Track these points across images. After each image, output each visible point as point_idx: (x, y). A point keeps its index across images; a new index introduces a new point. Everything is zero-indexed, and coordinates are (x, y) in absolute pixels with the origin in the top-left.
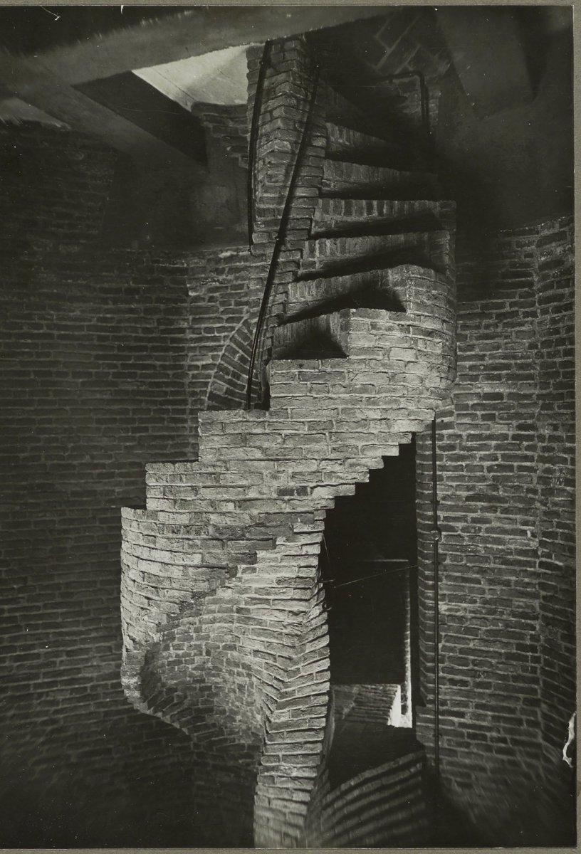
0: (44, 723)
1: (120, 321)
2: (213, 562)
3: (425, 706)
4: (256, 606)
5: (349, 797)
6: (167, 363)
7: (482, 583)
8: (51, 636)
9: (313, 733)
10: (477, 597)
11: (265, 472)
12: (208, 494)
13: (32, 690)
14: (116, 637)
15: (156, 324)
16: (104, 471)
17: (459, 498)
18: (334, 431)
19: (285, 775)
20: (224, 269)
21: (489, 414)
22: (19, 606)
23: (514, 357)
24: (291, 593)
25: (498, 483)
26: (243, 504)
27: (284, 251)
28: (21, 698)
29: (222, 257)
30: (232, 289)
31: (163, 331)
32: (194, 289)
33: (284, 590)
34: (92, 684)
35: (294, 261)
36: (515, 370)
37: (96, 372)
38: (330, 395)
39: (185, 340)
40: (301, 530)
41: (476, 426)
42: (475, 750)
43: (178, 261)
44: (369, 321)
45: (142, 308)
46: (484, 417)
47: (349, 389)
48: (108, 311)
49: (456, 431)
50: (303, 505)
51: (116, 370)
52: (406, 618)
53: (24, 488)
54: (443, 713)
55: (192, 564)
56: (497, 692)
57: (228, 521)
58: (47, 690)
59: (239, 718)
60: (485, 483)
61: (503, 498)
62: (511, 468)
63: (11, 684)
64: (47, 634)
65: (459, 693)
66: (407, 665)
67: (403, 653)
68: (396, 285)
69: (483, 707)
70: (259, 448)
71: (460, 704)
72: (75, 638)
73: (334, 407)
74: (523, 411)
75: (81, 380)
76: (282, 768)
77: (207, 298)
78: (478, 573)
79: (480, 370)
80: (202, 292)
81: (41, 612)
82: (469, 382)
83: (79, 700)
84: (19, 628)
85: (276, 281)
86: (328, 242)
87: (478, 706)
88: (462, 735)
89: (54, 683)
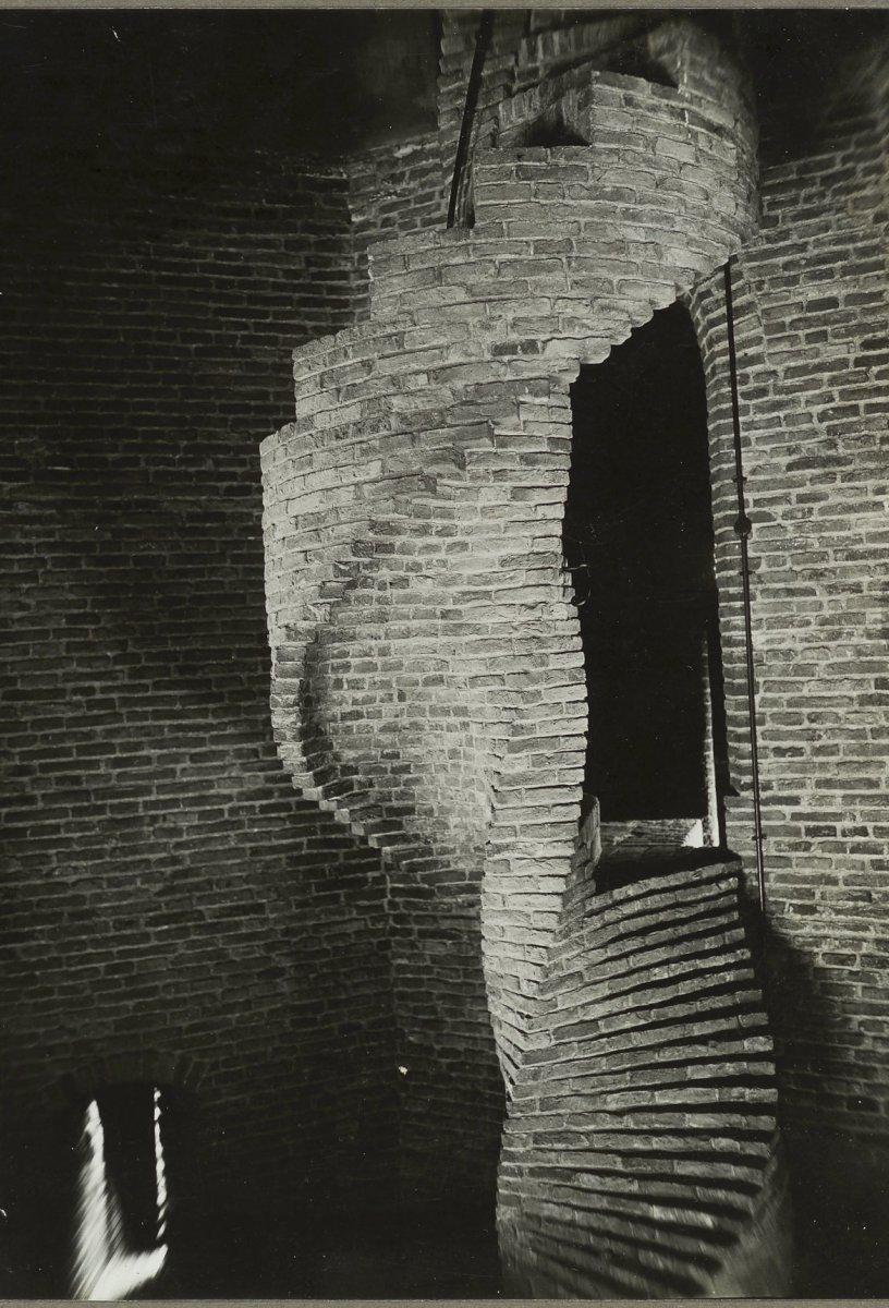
0: (162, 862)
1: (247, 259)
2: (399, 468)
3: (738, 795)
4: (470, 605)
5: (627, 909)
6: (324, 324)
7: (818, 593)
8: (166, 730)
9: (566, 790)
10: (811, 616)
11: (473, 321)
12: (386, 368)
13: (141, 812)
14: (264, 735)
15: (303, 265)
16: (235, 483)
17: (776, 467)
18: (574, 254)
19: (526, 856)
20: (403, 174)
21: (817, 332)
22: (119, 683)
23: (852, 239)
24: (523, 578)
25: (836, 437)
26: (440, 374)
27: (491, 59)
28: (127, 822)
29: (400, 156)
30: (416, 203)
31: (315, 276)
32: (360, 212)
33: (512, 574)
34: (230, 805)
35: (506, 70)
36: (855, 260)
37: (217, 335)
38: (565, 202)
39: (349, 290)
40: (534, 484)
41: (798, 354)
42: (819, 853)
43: (333, 169)
44: (620, 92)
45: (283, 240)
46: (810, 338)
47: (596, 193)
48: (231, 243)
49: (768, 366)
50: (532, 367)
51: (246, 333)
52: (706, 718)
53: (117, 505)
54: (767, 802)
55: (367, 478)
56: (848, 759)
57: (420, 404)
58: (163, 812)
59: (453, 820)
60: (816, 439)
61: (845, 458)
62: (854, 410)
63: (109, 802)
64: (161, 728)
65: (790, 767)
66: (709, 791)
67: (703, 772)
68: (660, 53)
69: (828, 783)
70: (462, 284)
71: (791, 784)
72: (202, 734)
73: (572, 219)
74: (870, 319)
75: (194, 346)
76: (521, 845)
77: (379, 222)
78: (810, 578)
79: (800, 266)
80: (372, 214)
81: (149, 694)
82: (785, 288)
83: (213, 828)
84: (117, 717)
85: (480, 106)
86: (556, 37)
87: (819, 784)
88: (797, 832)
89: (174, 803)
